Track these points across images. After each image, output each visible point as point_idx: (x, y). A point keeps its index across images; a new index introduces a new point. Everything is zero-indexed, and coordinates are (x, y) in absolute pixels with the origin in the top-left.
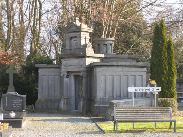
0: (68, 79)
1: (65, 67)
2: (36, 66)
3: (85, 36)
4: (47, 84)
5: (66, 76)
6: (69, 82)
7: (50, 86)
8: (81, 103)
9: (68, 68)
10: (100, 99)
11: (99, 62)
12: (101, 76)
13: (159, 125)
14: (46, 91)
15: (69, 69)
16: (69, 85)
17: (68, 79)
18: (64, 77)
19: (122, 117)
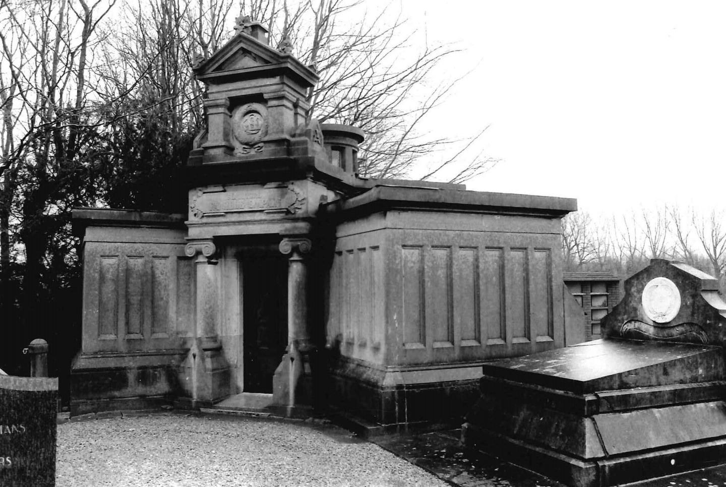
1: (205, 220)
18: (201, 259)
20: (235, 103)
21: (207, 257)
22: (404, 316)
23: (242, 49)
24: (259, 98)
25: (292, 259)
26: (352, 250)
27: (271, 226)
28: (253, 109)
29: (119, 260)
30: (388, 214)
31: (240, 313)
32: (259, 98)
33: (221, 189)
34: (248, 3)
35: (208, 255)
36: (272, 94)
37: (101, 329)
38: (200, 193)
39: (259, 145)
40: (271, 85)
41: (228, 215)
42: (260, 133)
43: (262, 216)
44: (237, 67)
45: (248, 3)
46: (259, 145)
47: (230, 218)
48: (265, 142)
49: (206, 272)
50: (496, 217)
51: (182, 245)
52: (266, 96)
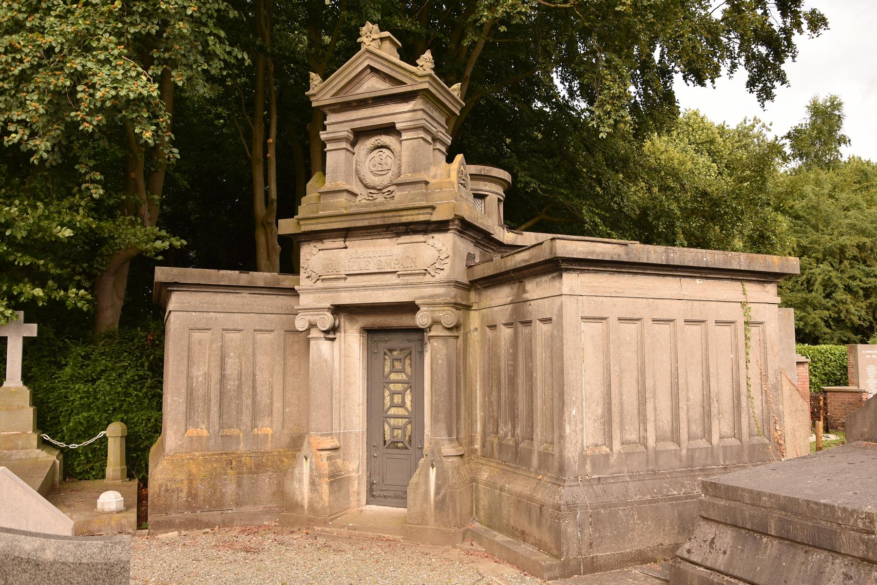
0: (333, 348)
1: (320, 284)
2: (35, 326)
3: (554, 318)
4: (215, 376)
5: (326, 332)
6: (336, 365)
7: (231, 385)
8: (427, 476)
9: (337, 289)
10: (583, 458)
11: (69, 533)
12: (585, 326)
13: (103, 42)
14: (209, 410)
15: (343, 294)
16: (336, 376)
17: (333, 348)
18: (314, 333)
19: (354, 66)
20: (360, 134)
21: (324, 332)
22: (479, 414)
23: (369, 67)
24: (390, 129)
25: (431, 334)
26: (550, 320)
27: (404, 291)
28: (382, 143)
29: (212, 334)
30: (565, 275)
31: (363, 404)
32: (390, 129)
33: (342, 244)
34: (2, 200)
35: (324, 329)
36: (409, 124)
37: (189, 418)
38: (315, 251)
39: (389, 189)
40: (405, 112)
41: (350, 279)
42: (390, 173)
43: (392, 279)
44: (359, 91)
45: (2, 200)
46: (389, 189)
47: (351, 281)
48: (398, 185)
49: (321, 348)
50: (698, 281)
51: (291, 316)
52: (398, 126)
